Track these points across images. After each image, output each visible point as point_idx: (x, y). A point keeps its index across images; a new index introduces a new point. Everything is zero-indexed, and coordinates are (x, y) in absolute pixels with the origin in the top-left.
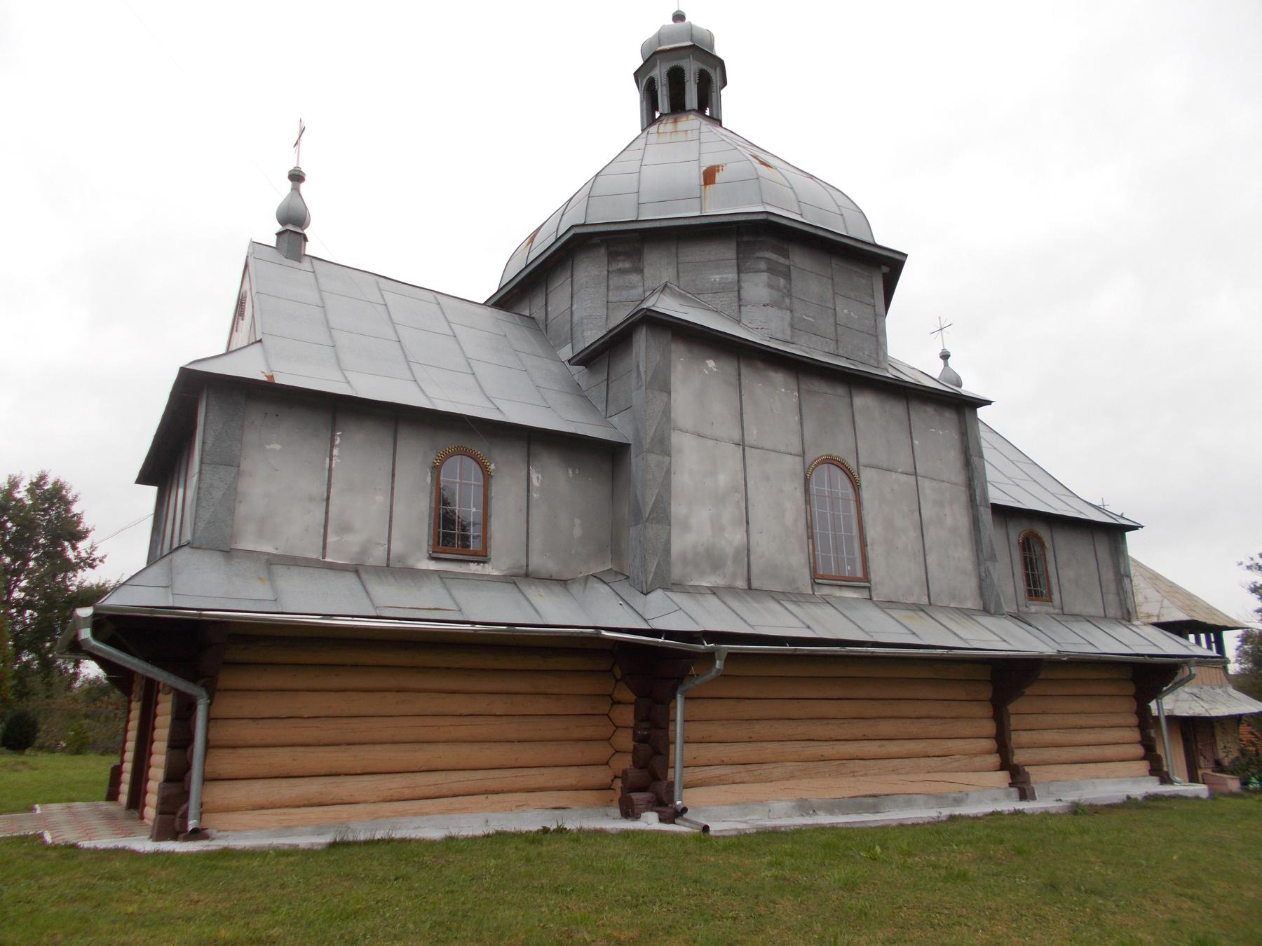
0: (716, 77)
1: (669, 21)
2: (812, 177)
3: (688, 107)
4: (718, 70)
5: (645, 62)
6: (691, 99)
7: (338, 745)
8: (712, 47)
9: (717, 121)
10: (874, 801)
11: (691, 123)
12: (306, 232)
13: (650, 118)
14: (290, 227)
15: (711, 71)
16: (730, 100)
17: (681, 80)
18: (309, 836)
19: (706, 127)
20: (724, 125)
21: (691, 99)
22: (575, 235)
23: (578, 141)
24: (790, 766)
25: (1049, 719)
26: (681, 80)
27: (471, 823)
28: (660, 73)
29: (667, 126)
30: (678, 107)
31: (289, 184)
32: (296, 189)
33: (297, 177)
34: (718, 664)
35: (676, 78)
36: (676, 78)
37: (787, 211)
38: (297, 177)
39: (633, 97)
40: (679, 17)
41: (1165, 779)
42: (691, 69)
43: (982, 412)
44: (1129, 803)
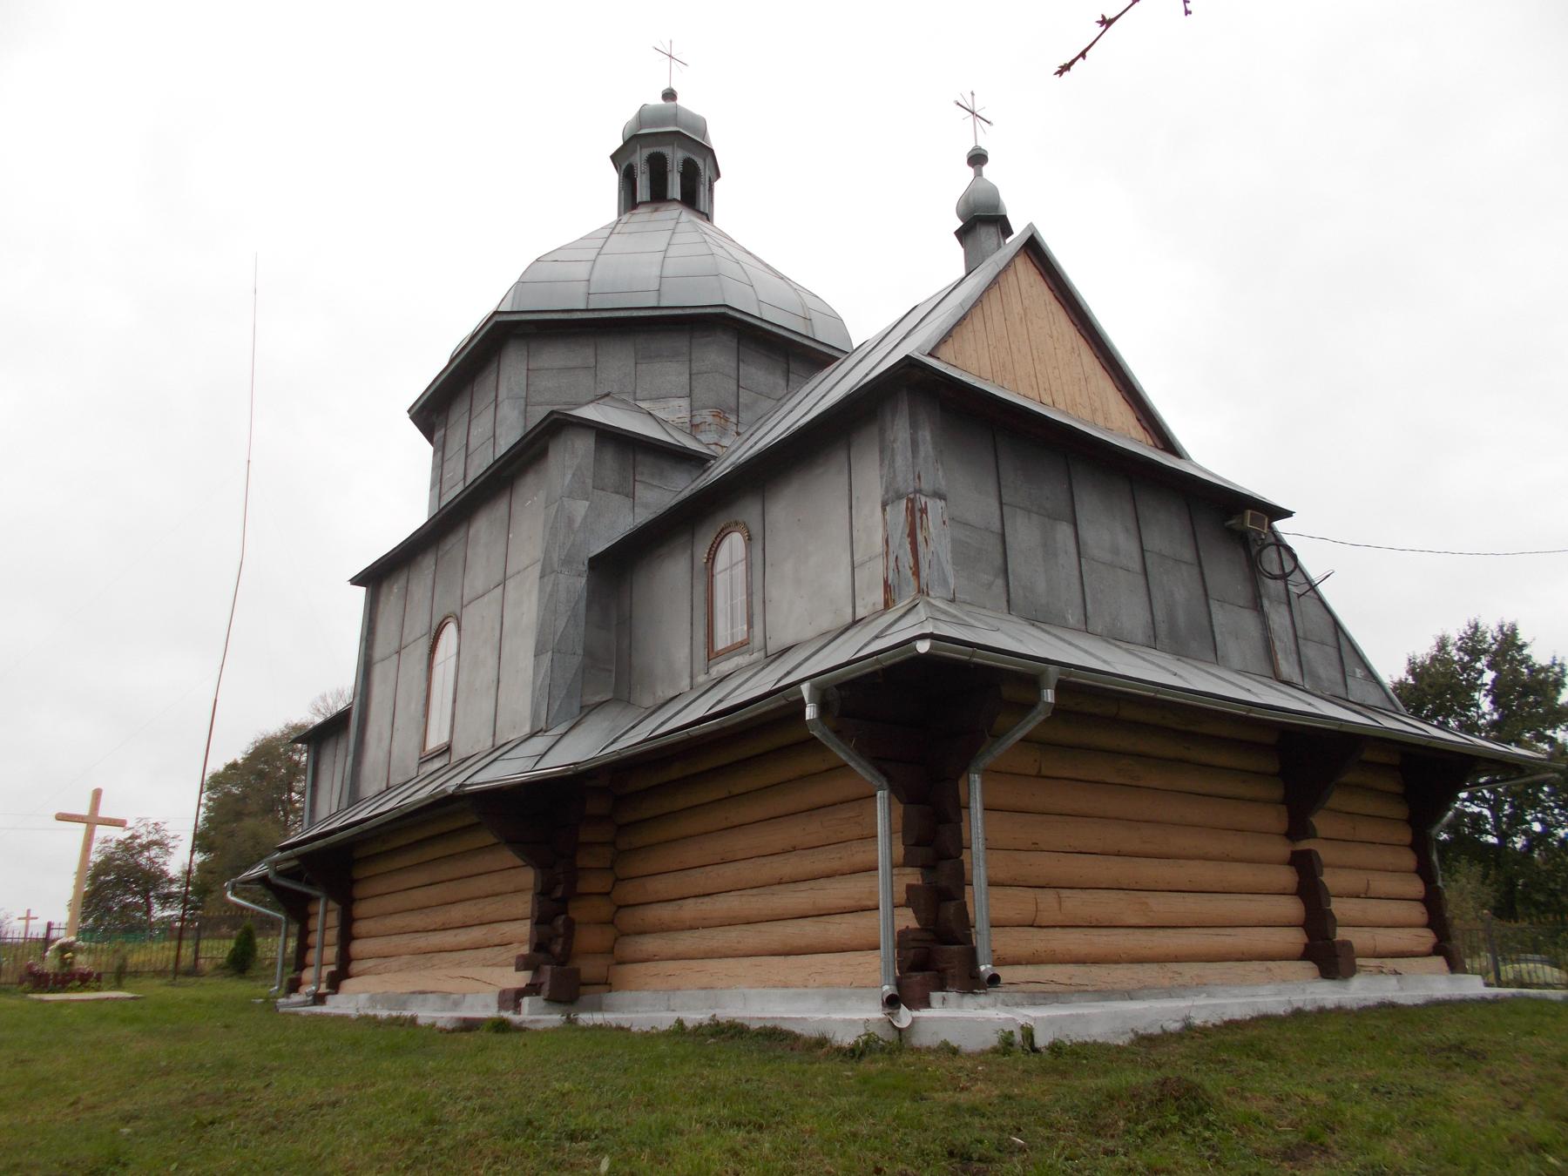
0: (706, 173)
1: (656, 100)
2: (782, 278)
3: (670, 196)
4: (709, 160)
5: (626, 143)
6: (675, 189)
8: (704, 133)
9: (708, 217)
11: (675, 215)
16: (725, 196)
17: (665, 166)
19: (686, 216)
21: (675, 189)
22: (497, 323)
24: (406, 958)
25: (729, 872)
26: (665, 166)
27: (1160, 1011)
28: (640, 159)
29: (642, 214)
30: (659, 196)
33: (977, 159)
37: (742, 301)
38: (977, 159)
39: (611, 179)
40: (669, 95)
41: (1329, 958)
42: (675, 157)
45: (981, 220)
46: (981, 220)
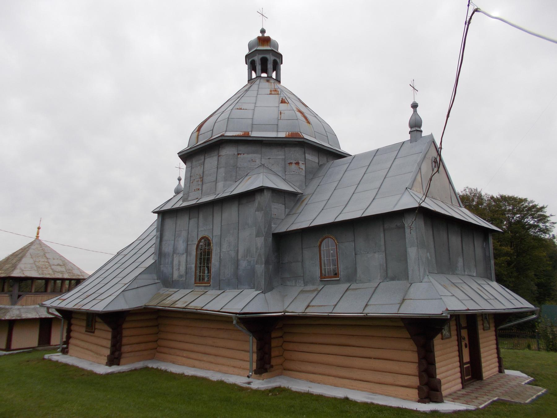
17: (264, 59)
26: (264, 59)
28: (257, 58)
31: (412, 110)
32: (415, 111)
33: (415, 106)
35: (264, 61)
38: (415, 106)
42: (271, 58)
45: (416, 126)
46: (416, 126)
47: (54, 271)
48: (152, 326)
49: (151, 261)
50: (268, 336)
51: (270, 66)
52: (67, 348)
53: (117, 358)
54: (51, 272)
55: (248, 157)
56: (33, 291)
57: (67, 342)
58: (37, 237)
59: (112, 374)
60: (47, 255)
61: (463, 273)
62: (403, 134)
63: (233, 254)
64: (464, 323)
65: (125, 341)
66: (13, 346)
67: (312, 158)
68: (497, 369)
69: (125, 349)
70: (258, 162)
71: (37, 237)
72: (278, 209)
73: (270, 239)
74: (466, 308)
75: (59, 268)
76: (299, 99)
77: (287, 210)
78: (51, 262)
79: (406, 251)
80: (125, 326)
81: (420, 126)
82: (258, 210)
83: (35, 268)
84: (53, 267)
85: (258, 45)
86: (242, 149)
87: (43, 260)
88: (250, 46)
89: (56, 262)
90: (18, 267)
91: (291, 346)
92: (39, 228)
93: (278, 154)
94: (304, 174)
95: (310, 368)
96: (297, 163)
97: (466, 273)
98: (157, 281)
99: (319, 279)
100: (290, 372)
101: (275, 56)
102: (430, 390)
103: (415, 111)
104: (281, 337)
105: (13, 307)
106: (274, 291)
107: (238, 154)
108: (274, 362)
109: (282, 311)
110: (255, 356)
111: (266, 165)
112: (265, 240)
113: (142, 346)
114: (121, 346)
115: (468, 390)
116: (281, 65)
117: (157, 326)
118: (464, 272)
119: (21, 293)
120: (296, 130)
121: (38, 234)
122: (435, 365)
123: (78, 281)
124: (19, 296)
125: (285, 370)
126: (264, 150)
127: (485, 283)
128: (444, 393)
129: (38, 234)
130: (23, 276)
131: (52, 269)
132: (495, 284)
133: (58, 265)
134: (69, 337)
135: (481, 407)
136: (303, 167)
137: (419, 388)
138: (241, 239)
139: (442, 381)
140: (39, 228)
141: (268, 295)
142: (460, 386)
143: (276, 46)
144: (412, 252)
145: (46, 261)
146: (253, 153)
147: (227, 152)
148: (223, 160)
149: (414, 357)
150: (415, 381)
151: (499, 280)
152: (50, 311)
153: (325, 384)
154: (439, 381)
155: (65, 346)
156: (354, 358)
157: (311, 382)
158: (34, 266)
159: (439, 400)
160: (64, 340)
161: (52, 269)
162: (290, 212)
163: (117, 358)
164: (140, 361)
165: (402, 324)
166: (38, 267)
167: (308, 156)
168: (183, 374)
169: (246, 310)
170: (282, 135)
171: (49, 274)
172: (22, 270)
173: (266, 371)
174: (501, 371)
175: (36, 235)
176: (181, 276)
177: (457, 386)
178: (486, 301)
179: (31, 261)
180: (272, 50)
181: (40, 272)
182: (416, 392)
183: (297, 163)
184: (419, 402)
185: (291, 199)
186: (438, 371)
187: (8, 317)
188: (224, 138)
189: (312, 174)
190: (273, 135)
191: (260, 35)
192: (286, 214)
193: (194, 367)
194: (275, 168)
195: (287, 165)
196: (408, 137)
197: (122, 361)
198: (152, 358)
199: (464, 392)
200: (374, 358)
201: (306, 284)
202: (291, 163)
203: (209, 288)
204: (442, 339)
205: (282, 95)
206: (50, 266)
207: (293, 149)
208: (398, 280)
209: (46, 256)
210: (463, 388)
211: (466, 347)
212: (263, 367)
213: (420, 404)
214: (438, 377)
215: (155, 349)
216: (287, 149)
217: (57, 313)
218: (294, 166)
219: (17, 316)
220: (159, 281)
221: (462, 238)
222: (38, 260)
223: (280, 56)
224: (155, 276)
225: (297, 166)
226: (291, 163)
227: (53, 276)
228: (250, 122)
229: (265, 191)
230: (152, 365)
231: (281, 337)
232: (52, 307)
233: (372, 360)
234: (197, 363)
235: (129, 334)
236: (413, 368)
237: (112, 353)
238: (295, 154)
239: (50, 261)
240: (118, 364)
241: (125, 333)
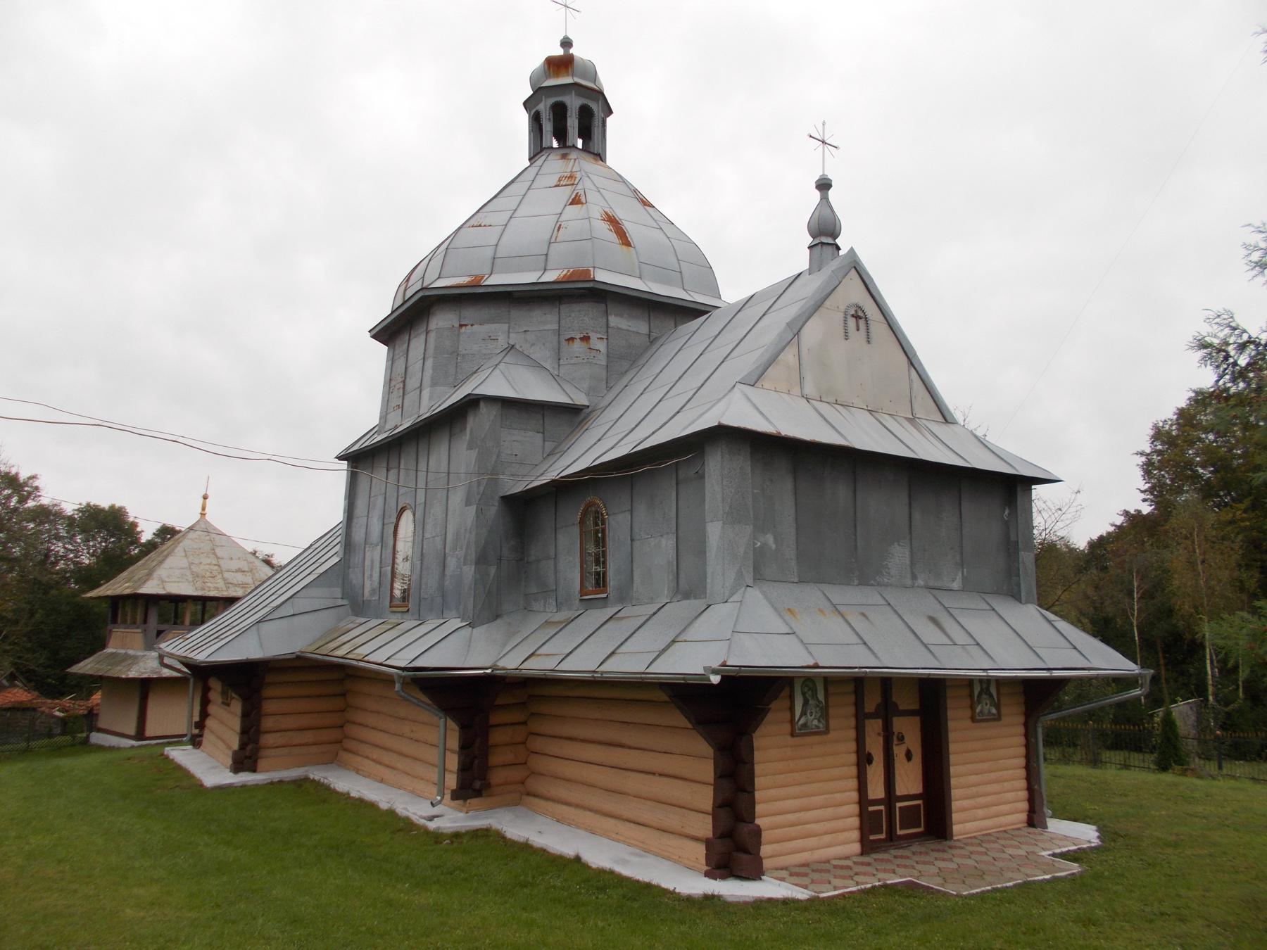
7: (654, 774)
10: (624, 862)
12: (838, 241)
13: (538, 150)
14: (825, 240)
15: (593, 106)
17: (567, 111)
18: (802, 894)
20: (610, 160)
23: (451, 170)
26: (567, 111)
28: (544, 107)
31: (817, 194)
32: (824, 198)
33: (824, 185)
34: (397, 687)
35: (559, 111)
36: (559, 111)
38: (824, 185)
42: (574, 103)
43: (1038, 491)
44: (786, 902)
45: (824, 232)
46: (824, 232)
47: (228, 584)
48: (330, 696)
49: (335, 560)
50: (488, 720)
51: (573, 123)
52: (201, 736)
53: (250, 757)
54: (221, 584)
55: (484, 331)
56: (187, 622)
57: (201, 725)
58: (203, 515)
59: (244, 787)
60: (219, 552)
61: (908, 582)
62: (794, 254)
63: (438, 540)
64: (906, 700)
65: (267, 723)
66: (148, 733)
67: (625, 323)
68: (1024, 816)
69: (267, 739)
70: (502, 341)
71: (203, 515)
72: (521, 440)
73: (493, 510)
74: (811, 663)
75: (239, 578)
76: (635, 191)
77: (549, 445)
78: (225, 564)
79: (704, 530)
80: (267, 692)
81: (835, 235)
82: (470, 447)
83: (190, 579)
84: (226, 575)
85: (548, 77)
86: (470, 313)
87: (209, 561)
88: (534, 80)
89: (235, 565)
90: (155, 575)
91: (537, 744)
92: (205, 497)
93: (543, 321)
94: (604, 363)
95: (576, 795)
96: (586, 339)
97: (921, 582)
98: (340, 602)
99: (578, 596)
100: (537, 800)
101: (583, 96)
102: (734, 849)
103: (824, 198)
104: (525, 723)
105: (147, 653)
106: (498, 621)
107: (461, 326)
108: (497, 777)
109: (488, 665)
110: (453, 762)
111: (517, 347)
112: (480, 511)
113: (309, 737)
114: (258, 733)
115: (866, 859)
116: (610, 121)
117: (344, 695)
118: (914, 577)
119: (162, 627)
120: (585, 264)
121: (204, 509)
122: (752, 793)
123: (231, 601)
124: (159, 633)
125: (523, 794)
126: (515, 313)
127: (985, 606)
128: (767, 863)
129: (204, 509)
130: (162, 592)
131: (224, 579)
132: (1032, 610)
133: (240, 570)
134: (204, 714)
135: (822, 895)
136: (601, 346)
137: (708, 843)
138: (443, 512)
139: (763, 834)
140: (205, 497)
141: (480, 631)
142: (856, 847)
143: (594, 77)
144: (715, 532)
145: (214, 562)
146: (492, 321)
147: (441, 321)
148: (432, 336)
149: (706, 770)
150: (704, 826)
151: (1045, 602)
152: (166, 661)
153: (578, 827)
154: (758, 832)
155: (196, 731)
156: (629, 773)
157: (558, 821)
158: (188, 573)
159: (754, 873)
160: (196, 718)
161: (224, 579)
162: (555, 448)
163: (250, 757)
164: (287, 768)
165: (663, 697)
166: (196, 575)
167: (614, 321)
168: (348, 794)
169: (419, 663)
170: (550, 276)
171: (217, 589)
172: (163, 581)
173: (478, 793)
174: (1034, 819)
175: (200, 510)
176: (373, 591)
177: (848, 846)
178: (923, 648)
179: (184, 563)
180: (576, 84)
181: (199, 584)
182: (701, 849)
183: (586, 339)
184: (707, 874)
185: (570, 416)
186: (759, 808)
187: (132, 674)
188: (428, 293)
189: (624, 362)
190: (529, 278)
191: (559, 52)
192: (547, 451)
193: (382, 781)
194: (538, 353)
195: (564, 343)
196: (802, 261)
197: (262, 763)
198: (332, 760)
199: (862, 859)
200: (660, 775)
201: (559, 607)
202: (572, 339)
203: (406, 616)
204: (792, 735)
205: (579, 187)
206: (221, 572)
207: (576, 307)
208: (695, 598)
209: (214, 554)
210: (862, 854)
211: (909, 756)
212: (473, 783)
213: (707, 879)
214: (758, 821)
215: (337, 744)
216: (565, 309)
217: (185, 670)
218: (577, 346)
219: (153, 672)
220: (345, 602)
221: (910, 496)
222: (197, 561)
223: (599, 95)
224: (338, 592)
225: (584, 345)
226: (572, 339)
227: (225, 594)
228: (489, 253)
229: (482, 404)
230: (317, 774)
231: (525, 723)
232: (171, 655)
233: (657, 778)
234: (387, 773)
235: (278, 709)
236: (705, 798)
237: (243, 746)
238: (581, 317)
239: (221, 562)
240: (254, 771)
241: (269, 707)
